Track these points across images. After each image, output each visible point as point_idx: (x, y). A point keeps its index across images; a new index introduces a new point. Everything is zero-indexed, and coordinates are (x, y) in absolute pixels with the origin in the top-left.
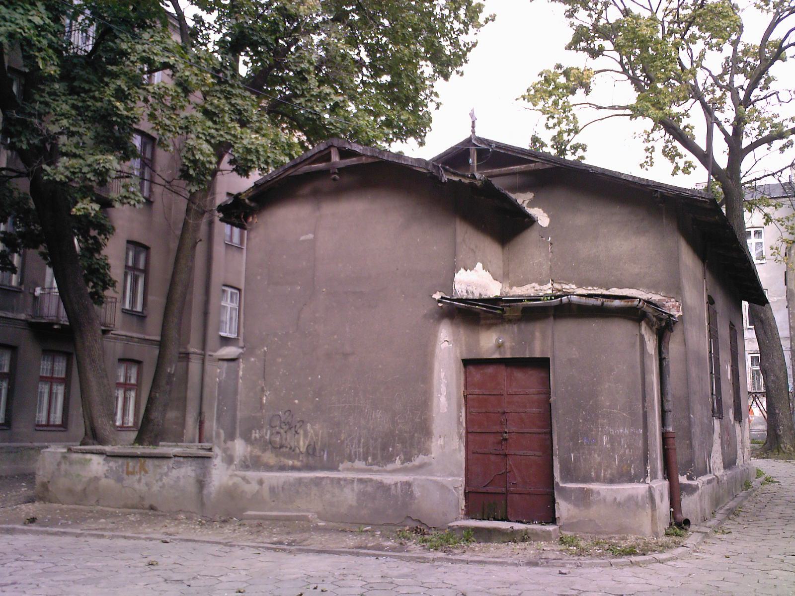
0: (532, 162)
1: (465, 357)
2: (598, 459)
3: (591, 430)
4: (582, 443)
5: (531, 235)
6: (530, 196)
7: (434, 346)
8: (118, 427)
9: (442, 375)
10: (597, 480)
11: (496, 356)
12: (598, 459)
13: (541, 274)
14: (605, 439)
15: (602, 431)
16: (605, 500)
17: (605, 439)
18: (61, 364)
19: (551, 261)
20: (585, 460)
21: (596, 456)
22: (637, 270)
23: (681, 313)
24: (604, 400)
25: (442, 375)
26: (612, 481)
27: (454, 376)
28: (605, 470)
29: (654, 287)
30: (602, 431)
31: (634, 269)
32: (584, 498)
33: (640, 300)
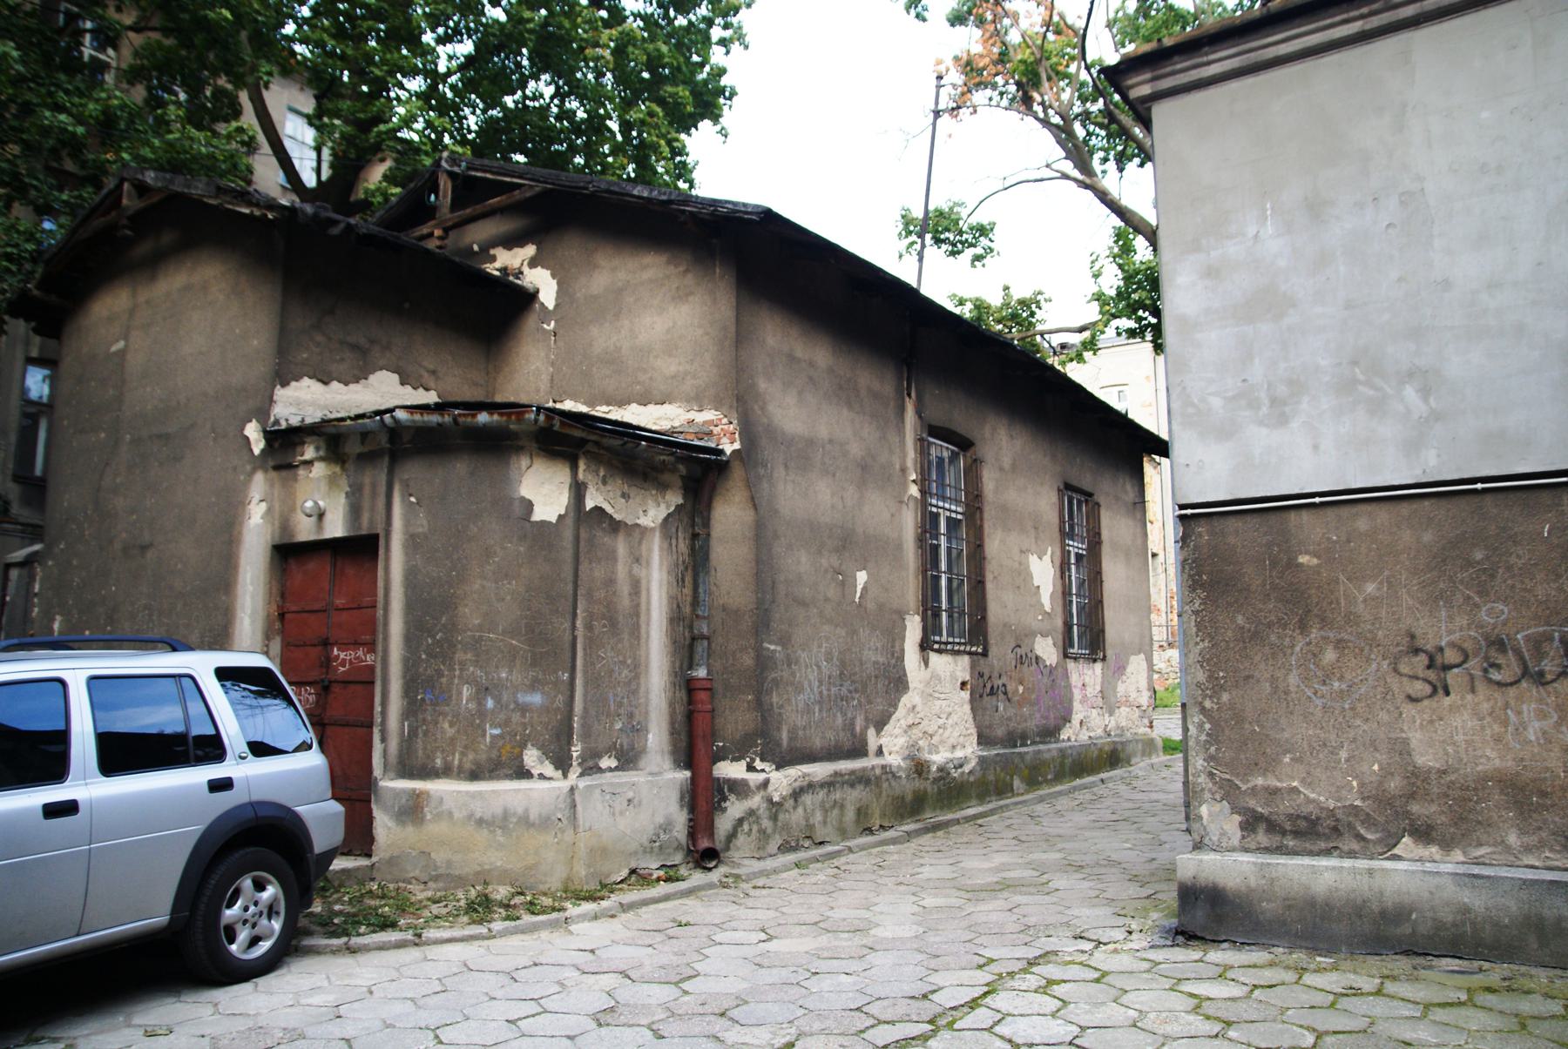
0: (519, 186)
1: (277, 541)
2: (450, 732)
3: (440, 674)
4: (423, 700)
5: (531, 322)
6: (530, 250)
7: (241, 524)
8: (523, 746)
9: (249, 576)
10: (446, 772)
11: (312, 537)
12: (450, 732)
13: (538, 391)
14: (466, 692)
15: (460, 677)
16: (450, 814)
17: (466, 692)
18: (1297, 731)
19: (553, 364)
20: (426, 733)
21: (446, 725)
22: (673, 369)
23: (737, 446)
24: (470, 616)
25: (249, 576)
26: (474, 776)
27: (262, 578)
28: (463, 754)
29: (698, 400)
30: (460, 677)
31: (668, 366)
32: (412, 810)
33: (539, 409)
